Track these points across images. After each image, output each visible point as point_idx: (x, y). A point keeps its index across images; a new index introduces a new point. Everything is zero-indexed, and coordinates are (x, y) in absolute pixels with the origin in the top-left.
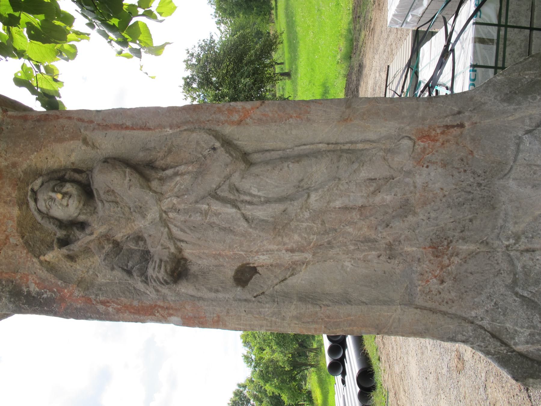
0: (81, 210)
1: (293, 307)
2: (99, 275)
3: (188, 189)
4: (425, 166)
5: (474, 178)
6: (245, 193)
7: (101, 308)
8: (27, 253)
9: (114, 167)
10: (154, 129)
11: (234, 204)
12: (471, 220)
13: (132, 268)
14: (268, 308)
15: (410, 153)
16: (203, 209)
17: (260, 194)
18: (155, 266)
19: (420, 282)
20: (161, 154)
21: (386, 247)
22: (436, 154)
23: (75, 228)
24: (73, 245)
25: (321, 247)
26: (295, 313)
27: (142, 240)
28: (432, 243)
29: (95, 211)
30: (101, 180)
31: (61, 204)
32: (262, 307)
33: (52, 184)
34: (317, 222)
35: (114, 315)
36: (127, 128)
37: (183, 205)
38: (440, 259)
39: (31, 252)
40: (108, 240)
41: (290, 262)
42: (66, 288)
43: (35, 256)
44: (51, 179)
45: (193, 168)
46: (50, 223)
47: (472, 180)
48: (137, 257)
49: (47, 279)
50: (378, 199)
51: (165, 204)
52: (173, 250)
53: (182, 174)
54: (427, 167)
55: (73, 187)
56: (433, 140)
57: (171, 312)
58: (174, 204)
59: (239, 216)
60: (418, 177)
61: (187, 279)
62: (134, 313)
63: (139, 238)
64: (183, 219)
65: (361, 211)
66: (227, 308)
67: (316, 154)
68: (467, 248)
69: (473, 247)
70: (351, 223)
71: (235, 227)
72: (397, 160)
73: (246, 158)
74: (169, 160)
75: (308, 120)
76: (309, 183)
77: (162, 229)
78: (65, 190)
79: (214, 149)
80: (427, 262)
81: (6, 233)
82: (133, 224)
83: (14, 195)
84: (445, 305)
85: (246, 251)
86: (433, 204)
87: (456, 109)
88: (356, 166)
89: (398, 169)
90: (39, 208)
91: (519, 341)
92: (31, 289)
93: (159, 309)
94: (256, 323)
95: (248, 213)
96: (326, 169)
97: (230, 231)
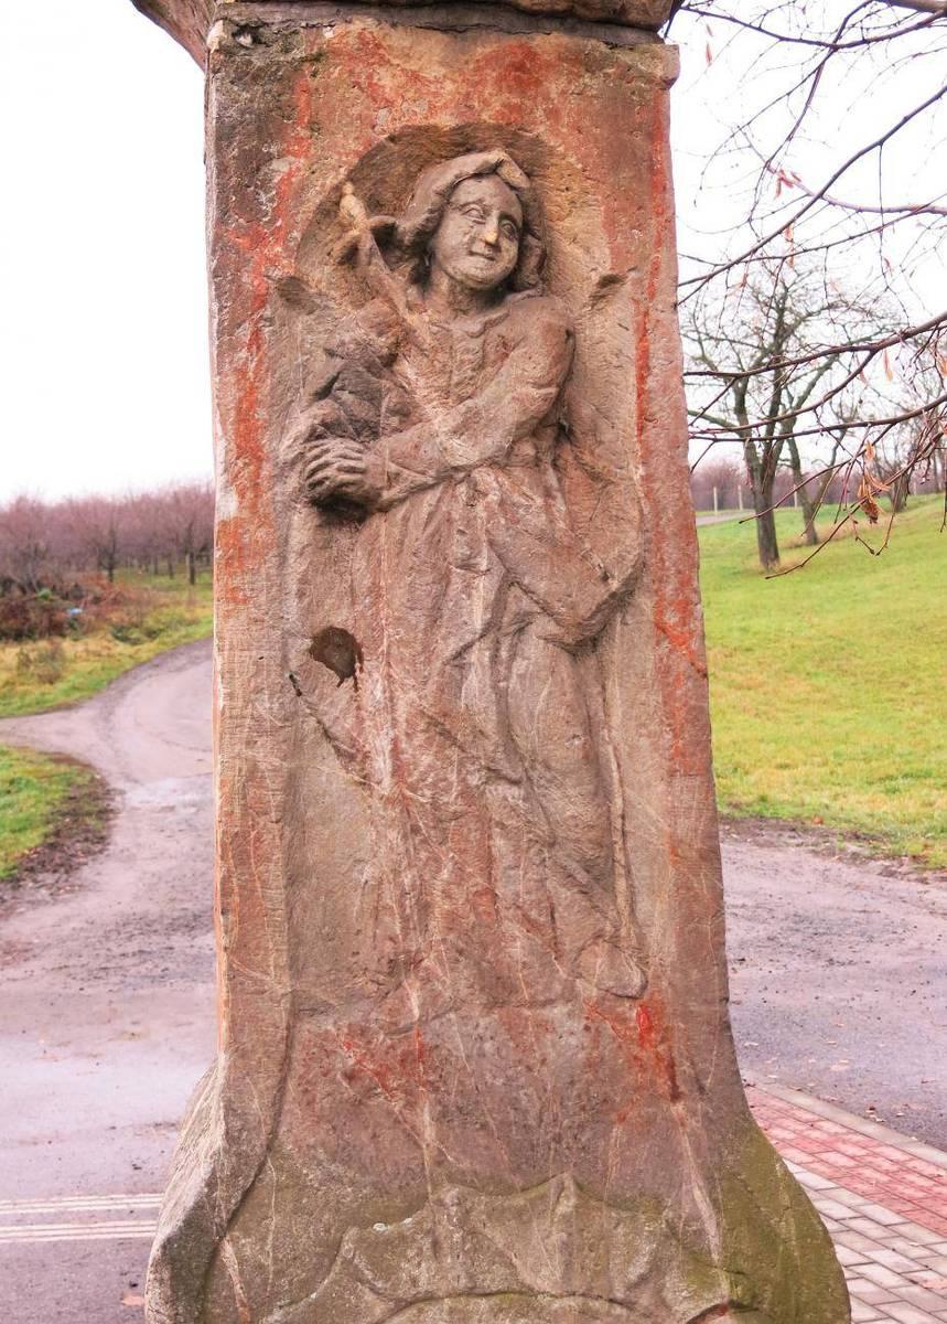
0: (462, 282)
1: (277, 762)
2: (312, 316)
3: (518, 522)
4: (589, 1023)
5: (570, 1127)
6: (513, 646)
7: (244, 333)
8: (356, 153)
9: (558, 359)
10: (640, 442)
11: (488, 628)
12: (484, 1126)
13: (336, 399)
14: (271, 709)
15: (614, 991)
16: (479, 559)
17: (514, 679)
18: (351, 459)
19: (346, 1030)
20: (587, 458)
21: (410, 952)
22: (615, 1045)
23: (416, 261)
24: (381, 263)
25: (405, 814)
26: (262, 766)
27: (401, 422)
28: (431, 1050)
29: (458, 311)
30: (529, 320)
31: (473, 240)
32: (271, 696)
33: (516, 211)
34: (459, 801)
35: (231, 363)
36: (642, 379)
37: (484, 515)
38: (399, 1068)
39: (361, 160)
40: (397, 344)
41: (367, 748)
42: (286, 249)
43: (352, 171)
44: (525, 206)
45: (560, 530)
46: (431, 211)
47: (566, 1122)
48: (363, 411)
49: (302, 203)
50: (513, 928)
51: (486, 478)
52: (386, 495)
53: (547, 508)
54: (587, 1028)
55: (510, 261)
56: (641, 1037)
57: (249, 495)
58: (486, 495)
59: (468, 638)
60: (565, 1010)
61: (320, 526)
62: (239, 410)
63: (406, 414)
64: (455, 516)
65: (486, 894)
66: (266, 618)
67: (601, 791)
68: (427, 1123)
69: (429, 1133)
70: (460, 875)
71: (443, 631)
72: (598, 961)
73: (585, 643)
74: (576, 474)
75: (672, 773)
76: (542, 782)
77: (432, 473)
78: (505, 244)
79: (605, 578)
80: (389, 1042)
81: (400, 101)
82: (435, 403)
83: (485, 116)
84: (300, 1088)
85: (388, 653)
86: (512, 1044)
87: (708, 1083)
88: (582, 877)
89: (579, 966)
90: (461, 186)
91: (243, 1245)
92: (275, 165)
93: (252, 467)
94: (238, 683)
95: (473, 657)
96: (573, 817)
97: (435, 618)
